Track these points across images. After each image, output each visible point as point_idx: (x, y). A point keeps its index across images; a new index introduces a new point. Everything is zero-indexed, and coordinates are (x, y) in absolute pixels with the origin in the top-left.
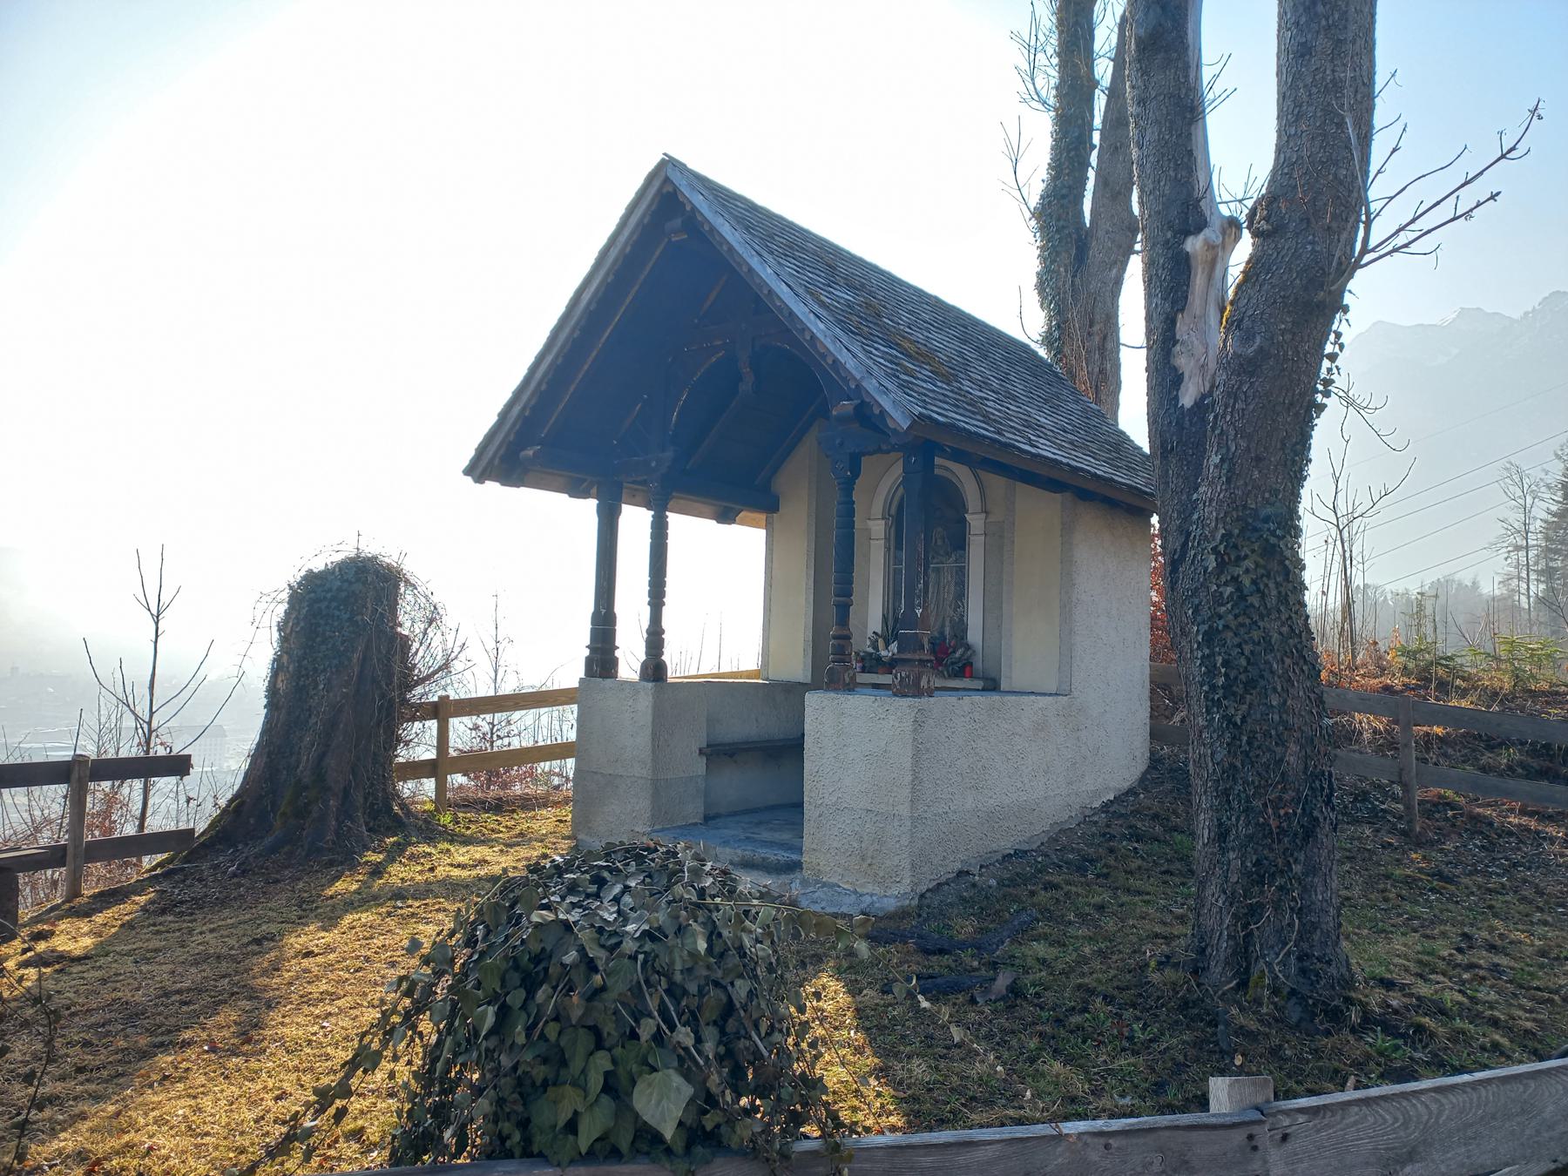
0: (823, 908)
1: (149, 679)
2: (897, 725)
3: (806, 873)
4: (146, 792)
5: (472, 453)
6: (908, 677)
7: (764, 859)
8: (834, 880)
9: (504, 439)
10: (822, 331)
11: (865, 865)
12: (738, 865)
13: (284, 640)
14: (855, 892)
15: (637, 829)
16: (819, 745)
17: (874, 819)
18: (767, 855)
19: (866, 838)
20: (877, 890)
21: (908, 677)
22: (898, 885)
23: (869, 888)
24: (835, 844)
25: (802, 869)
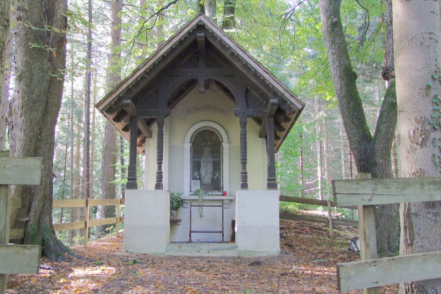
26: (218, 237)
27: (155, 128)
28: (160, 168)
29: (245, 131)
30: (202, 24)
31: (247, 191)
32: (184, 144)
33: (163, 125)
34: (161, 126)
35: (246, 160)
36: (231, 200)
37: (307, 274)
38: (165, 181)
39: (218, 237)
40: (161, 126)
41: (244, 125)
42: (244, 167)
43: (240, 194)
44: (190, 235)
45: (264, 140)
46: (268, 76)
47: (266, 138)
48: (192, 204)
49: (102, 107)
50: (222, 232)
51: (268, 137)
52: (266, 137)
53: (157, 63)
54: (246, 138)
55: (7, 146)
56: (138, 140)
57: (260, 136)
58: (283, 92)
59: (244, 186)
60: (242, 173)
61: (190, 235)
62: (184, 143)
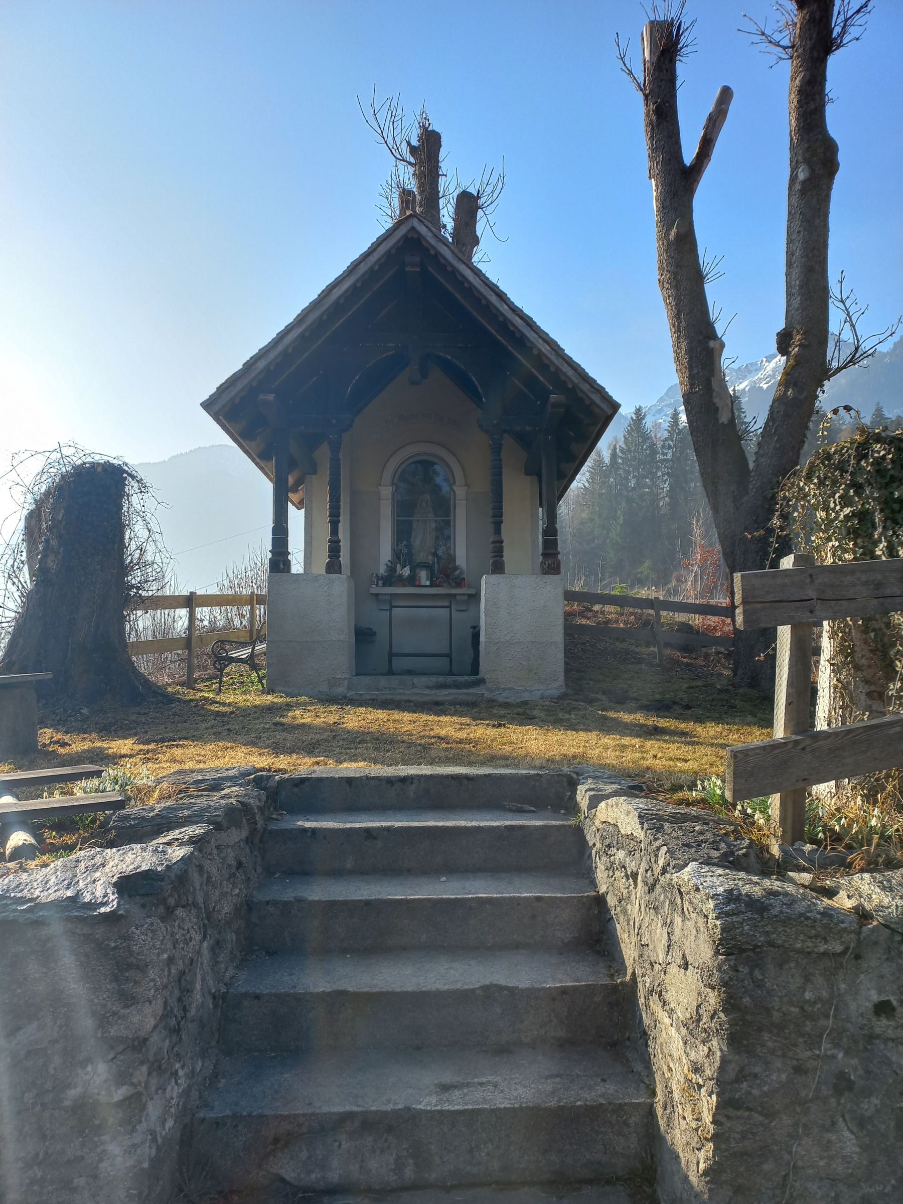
3: (489, 685)
5: (213, 390)
6: (553, 563)
14: (527, 690)
21: (553, 563)
26: (442, 663)
27: (323, 454)
28: (334, 531)
29: (501, 460)
30: (416, 236)
31: (502, 575)
32: (379, 487)
33: (340, 448)
34: (335, 449)
35: (501, 516)
36: (471, 596)
37: (645, 1192)
38: (344, 557)
39: (442, 663)
40: (335, 449)
41: (497, 449)
42: (498, 531)
43: (486, 583)
44: (390, 662)
45: (535, 478)
46: (548, 348)
47: (539, 475)
48: (394, 604)
49: (216, 407)
50: (449, 656)
51: (544, 477)
52: (539, 475)
53: (325, 317)
54: (500, 474)
55: (796, 349)
56: (291, 480)
57: (528, 473)
58: (576, 381)
59: (498, 568)
60: (494, 542)
61: (390, 662)
62: (380, 485)
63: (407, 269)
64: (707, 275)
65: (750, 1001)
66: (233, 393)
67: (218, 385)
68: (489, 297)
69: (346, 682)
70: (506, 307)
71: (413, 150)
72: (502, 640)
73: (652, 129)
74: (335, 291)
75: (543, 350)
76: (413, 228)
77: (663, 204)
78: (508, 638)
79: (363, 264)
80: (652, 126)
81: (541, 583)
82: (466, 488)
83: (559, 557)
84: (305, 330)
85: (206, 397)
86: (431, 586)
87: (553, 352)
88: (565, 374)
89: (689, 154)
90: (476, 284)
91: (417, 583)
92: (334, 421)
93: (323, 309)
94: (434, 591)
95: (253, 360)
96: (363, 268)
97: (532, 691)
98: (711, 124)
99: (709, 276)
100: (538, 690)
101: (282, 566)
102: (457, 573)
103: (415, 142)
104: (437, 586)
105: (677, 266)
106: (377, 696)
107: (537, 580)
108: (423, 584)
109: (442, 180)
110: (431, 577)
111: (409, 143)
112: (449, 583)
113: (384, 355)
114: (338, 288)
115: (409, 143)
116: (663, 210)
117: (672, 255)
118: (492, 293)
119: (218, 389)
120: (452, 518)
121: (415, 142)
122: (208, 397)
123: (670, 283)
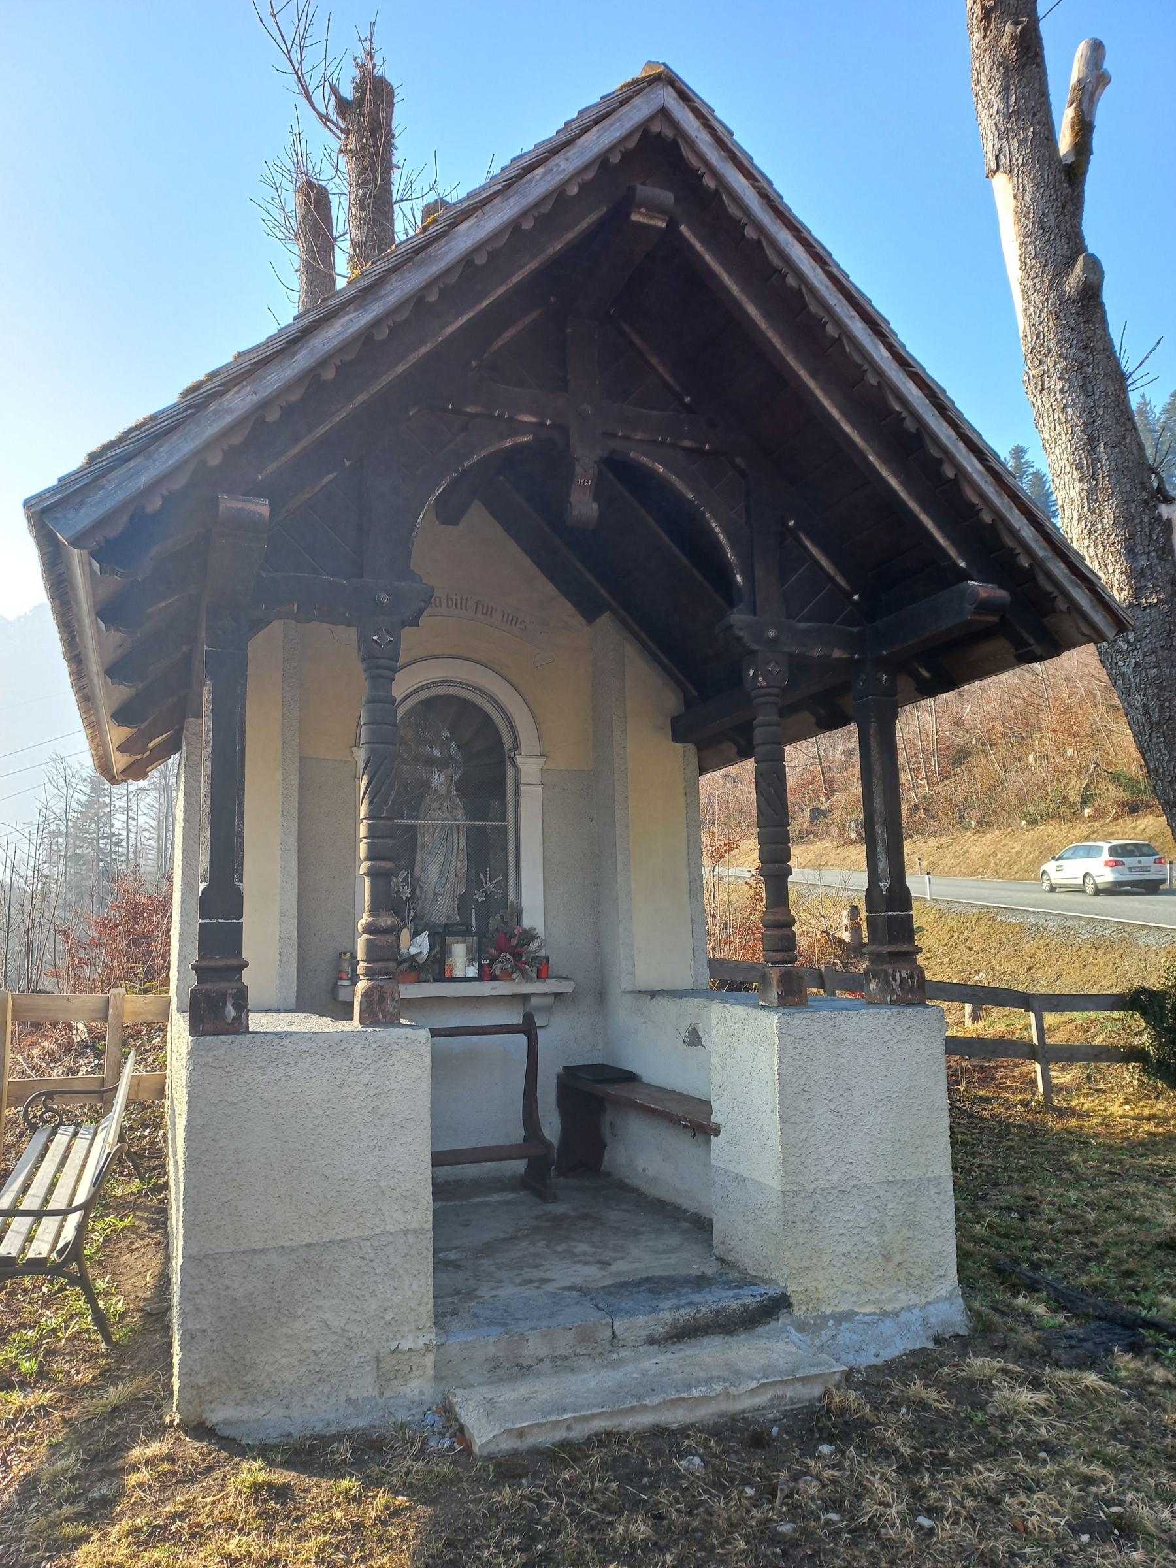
0: (877, 1356)
1: (523, 801)
2: (923, 1047)
3: (799, 1310)
4: (339, 275)
5: (74, 462)
6: (911, 977)
7: (717, 1312)
8: (844, 1307)
9: (812, 290)
10: (980, 472)
11: (891, 1267)
12: (666, 1340)
13: (753, 303)
14: (884, 1314)
15: (406, 1345)
16: (807, 1096)
17: (900, 1193)
18: (723, 1304)
19: (889, 1225)
20: (916, 1299)
21: (911, 977)
22: (942, 1280)
23: (904, 1299)
24: (841, 1249)
25: (790, 1305)
30: (669, 133)
46: (979, 466)
58: (1041, 553)
63: (635, 217)
64: (1131, 374)
65: (701, 1472)
66: (143, 481)
67: (94, 447)
68: (848, 322)
69: (430, 1359)
70: (885, 353)
71: (343, 106)
72: (823, 1184)
73: (1006, 75)
74: (463, 227)
75: (969, 469)
76: (663, 113)
77: (1041, 222)
78: (834, 1177)
79: (539, 171)
80: (1007, 69)
81: (898, 1029)
82: (542, 760)
83: (920, 959)
84: (376, 323)
85: (45, 478)
86: (479, 978)
87: (990, 478)
88: (1014, 533)
89: (1065, 142)
90: (817, 284)
91: (447, 974)
92: (384, 598)
93: (435, 269)
94: (486, 988)
95: (218, 380)
96: (540, 185)
97: (897, 1315)
98: (1087, 96)
99: (1135, 377)
100: (909, 1308)
101: (231, 1012)
102: (533, 946)
103: (347, 92)
104: (494, 978)
105: (1085, 348)
106: (569, 1428)
107: (892, 1022)
108: (459, 973)
109: (396, 176)
110: (475, 955)
111: (334, 90)
112: (523, 972)
113: (508, 443)
114: (472, 220)
115: (334, 90)
116: (1043, 234)
117: (1072, 323)
118: (854, 313)
119: (92, 458)
120: (510, 823)
121: (347, 92)
122: (54, 482)
123: (1068, 380)
